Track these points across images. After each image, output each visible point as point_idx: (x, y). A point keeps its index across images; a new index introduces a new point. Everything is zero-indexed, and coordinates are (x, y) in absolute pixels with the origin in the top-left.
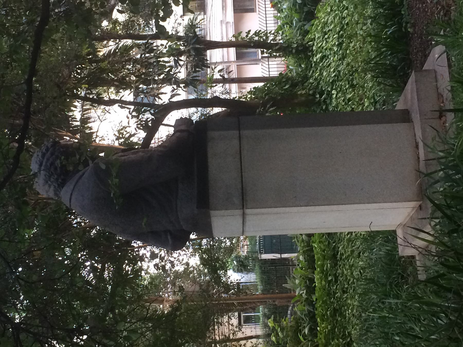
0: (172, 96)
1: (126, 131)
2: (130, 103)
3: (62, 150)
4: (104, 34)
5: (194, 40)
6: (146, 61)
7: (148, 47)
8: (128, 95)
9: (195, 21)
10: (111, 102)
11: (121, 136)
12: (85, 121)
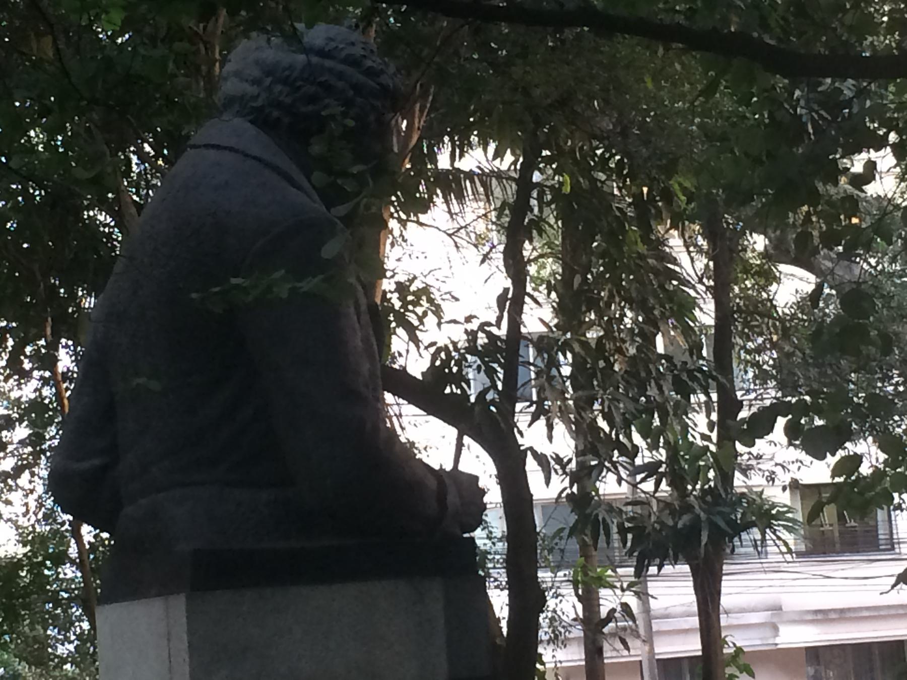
0: (541, 460)
1: (425, 314)
2: (515, 323)
3: (372, 118)
4: (731, 239)
5: (722, 524)
6: (649, 372)
7: (693, 378)
8: (538, 317)
9: (785, 527)
10: (516, 266)
11: (410, 298)
12: (452, 184)
